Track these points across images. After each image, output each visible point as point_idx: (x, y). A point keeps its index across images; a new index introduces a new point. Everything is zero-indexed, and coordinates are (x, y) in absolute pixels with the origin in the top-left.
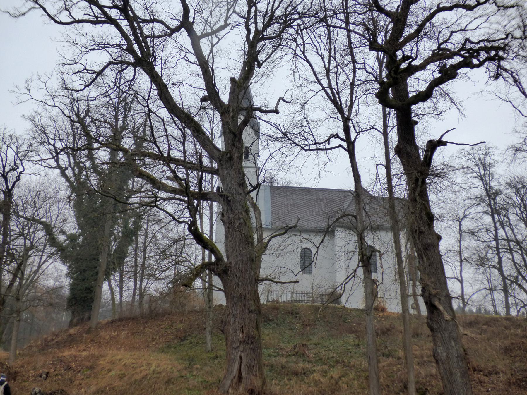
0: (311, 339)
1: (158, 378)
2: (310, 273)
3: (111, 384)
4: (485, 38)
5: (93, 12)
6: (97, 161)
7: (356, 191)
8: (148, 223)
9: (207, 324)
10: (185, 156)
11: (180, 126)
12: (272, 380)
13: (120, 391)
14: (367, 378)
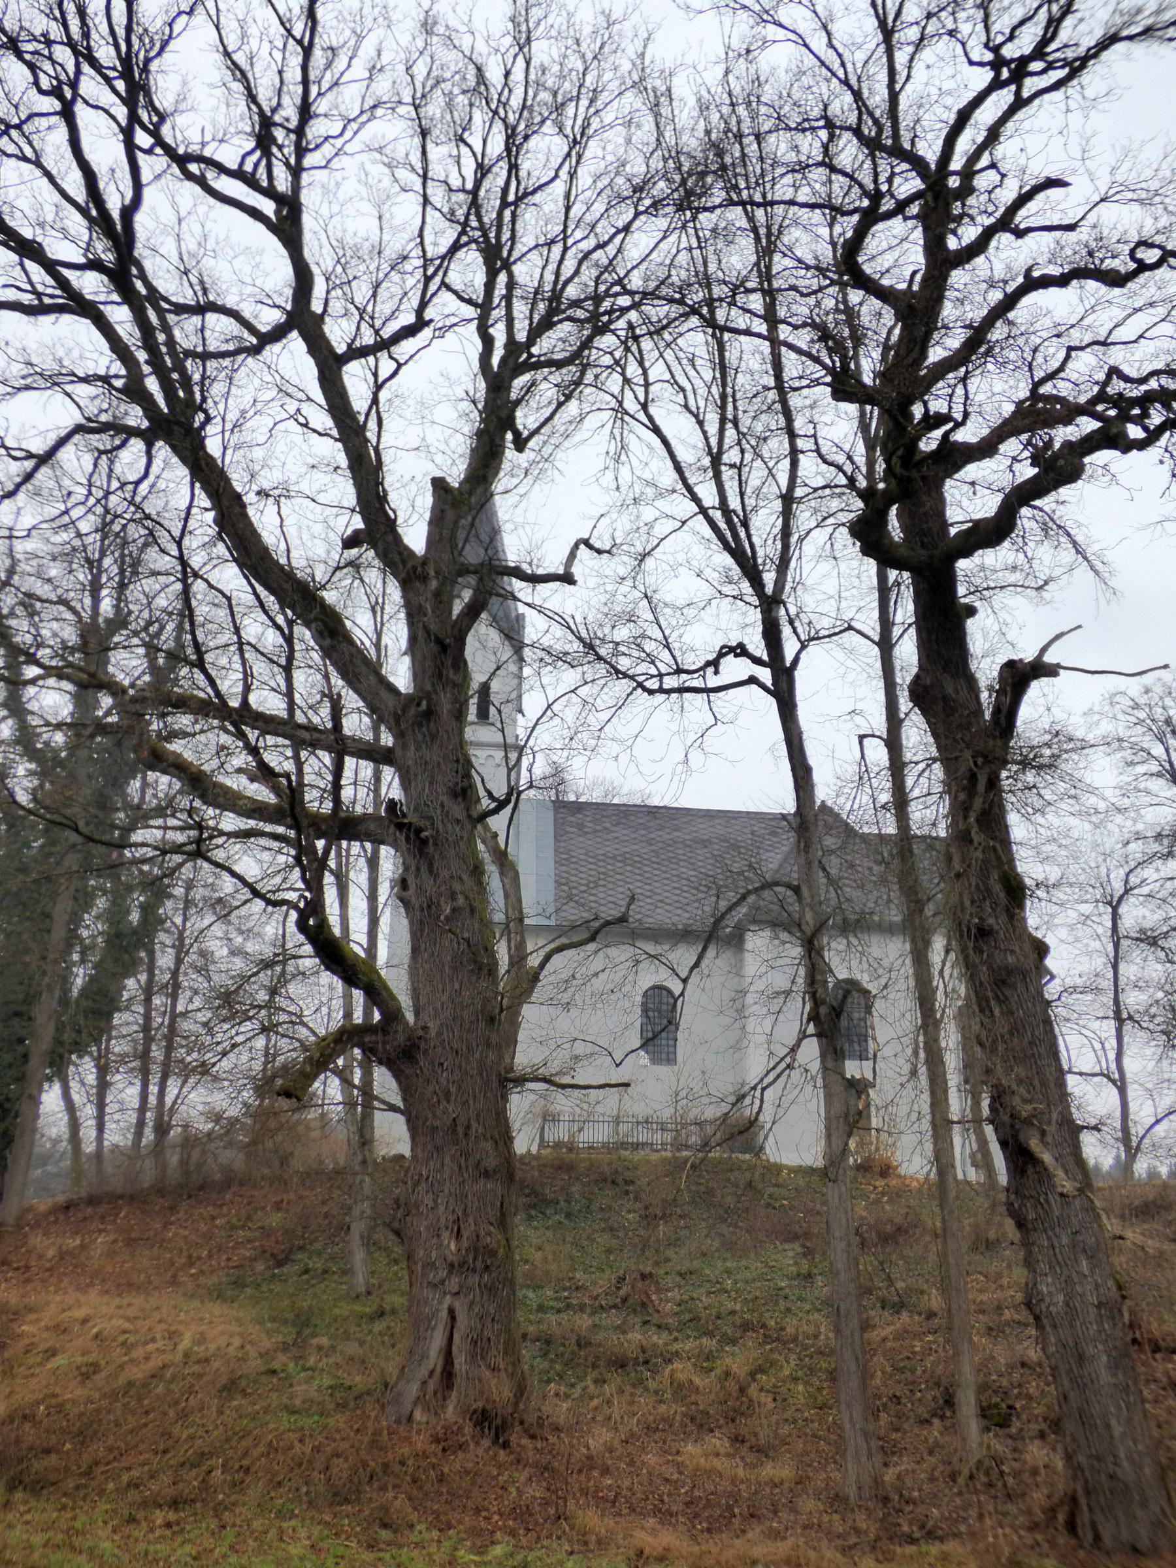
0: (667, 1260)
1: (200, 1376)
2: (671, 1060)
3: (55, 1396)
4: (1159, 365)
5: (30, 282)
6: (34, 721)
7: (799, 812)
8: (186, 909)
9: (356, 1212)
10: (291, 705)
11: (280, 620)
12: (548, 1382)
13: (82, 1414)
14: (833, 1376)
